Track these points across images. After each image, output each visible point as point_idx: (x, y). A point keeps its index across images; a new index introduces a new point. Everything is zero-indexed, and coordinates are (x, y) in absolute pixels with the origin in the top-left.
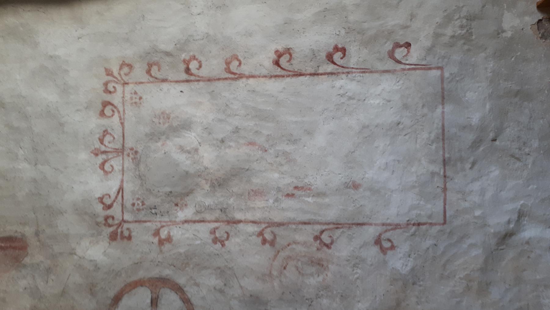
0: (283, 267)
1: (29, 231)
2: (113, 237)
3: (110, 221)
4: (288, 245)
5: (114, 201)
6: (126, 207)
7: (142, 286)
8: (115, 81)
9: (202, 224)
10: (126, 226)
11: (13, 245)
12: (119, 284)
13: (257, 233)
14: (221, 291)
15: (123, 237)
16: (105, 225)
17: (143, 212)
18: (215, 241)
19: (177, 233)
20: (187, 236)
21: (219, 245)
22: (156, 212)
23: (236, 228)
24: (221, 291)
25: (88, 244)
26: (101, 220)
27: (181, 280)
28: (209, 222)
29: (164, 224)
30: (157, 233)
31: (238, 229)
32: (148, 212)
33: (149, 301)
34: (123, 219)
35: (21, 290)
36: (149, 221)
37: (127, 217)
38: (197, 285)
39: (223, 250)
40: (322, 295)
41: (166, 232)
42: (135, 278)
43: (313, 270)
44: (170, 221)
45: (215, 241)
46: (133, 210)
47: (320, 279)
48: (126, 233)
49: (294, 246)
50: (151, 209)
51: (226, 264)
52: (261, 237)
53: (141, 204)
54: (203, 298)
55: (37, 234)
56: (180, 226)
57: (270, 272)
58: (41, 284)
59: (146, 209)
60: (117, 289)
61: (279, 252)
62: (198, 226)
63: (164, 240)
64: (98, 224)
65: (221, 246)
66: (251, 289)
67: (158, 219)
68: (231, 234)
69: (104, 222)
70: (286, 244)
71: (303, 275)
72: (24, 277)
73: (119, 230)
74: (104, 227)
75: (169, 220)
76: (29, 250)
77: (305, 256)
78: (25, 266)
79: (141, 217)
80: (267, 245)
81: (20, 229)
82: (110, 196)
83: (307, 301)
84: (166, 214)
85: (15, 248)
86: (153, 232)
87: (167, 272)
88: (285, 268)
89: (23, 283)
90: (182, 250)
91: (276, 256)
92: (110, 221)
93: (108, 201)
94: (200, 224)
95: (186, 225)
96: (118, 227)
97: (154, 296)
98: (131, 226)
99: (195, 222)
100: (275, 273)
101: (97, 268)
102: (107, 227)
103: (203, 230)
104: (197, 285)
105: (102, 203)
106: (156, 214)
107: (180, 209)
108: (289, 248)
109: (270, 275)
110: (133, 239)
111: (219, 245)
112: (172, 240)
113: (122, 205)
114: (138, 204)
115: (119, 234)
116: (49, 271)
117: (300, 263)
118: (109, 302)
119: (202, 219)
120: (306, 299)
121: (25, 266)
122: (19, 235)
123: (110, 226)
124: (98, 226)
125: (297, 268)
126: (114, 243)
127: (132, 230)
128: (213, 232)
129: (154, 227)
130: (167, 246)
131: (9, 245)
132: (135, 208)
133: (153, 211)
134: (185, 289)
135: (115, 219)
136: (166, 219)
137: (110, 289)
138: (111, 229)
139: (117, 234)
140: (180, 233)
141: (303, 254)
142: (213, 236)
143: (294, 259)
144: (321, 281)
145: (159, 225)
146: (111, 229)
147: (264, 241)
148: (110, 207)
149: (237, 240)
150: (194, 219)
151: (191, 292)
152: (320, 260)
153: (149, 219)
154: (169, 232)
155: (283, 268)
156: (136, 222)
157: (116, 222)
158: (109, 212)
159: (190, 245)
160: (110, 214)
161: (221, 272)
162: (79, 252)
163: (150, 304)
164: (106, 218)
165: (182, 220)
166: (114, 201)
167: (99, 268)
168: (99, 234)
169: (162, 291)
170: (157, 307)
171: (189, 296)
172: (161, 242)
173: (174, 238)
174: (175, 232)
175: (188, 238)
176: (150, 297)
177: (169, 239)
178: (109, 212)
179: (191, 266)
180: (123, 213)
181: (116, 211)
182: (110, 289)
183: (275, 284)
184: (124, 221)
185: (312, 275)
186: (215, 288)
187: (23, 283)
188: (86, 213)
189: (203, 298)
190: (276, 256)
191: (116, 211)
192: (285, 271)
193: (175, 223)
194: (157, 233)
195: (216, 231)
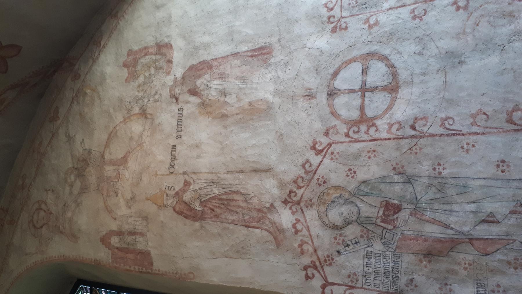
0: (476, 24)
1: (274, 40)
2: (334, 30)
3: (332, 19)
4: (481, 6)
5: (335, 5)
6: (343, 7)
7: (355, 62)
8: (85, 290)
9: (403, 8)
10: (343, 20)
11: (263, 52)
12: (337, 63)
13: (451, 3)
14: (420, 54)
15: (341, 29)
16: (328, 23)
17: (357, 9)
18: (414, 18)
19: (382, 18)
20: (391, 18)
21: (418, 20)
22: (367, 6)
23: (432, 5)
24: (420, 54)
25: (315, 38)
26: (325, 19)
27: (386, 51)
28: (409, 5)
29: (373, 13)
30: (367, 21)
31: (434, 4)
32: (361, 8)
33: (360, 71)
34: (341, 16)
35: (268, 81)
36: (361, 14)
37: (344, 14)
38: (399, 53)
39: (422, 23)
40: (514, 40)
41: (374, 19)
42: (349, 57)
43: (505, 21)
44: (377, 11)
45: (414, 18)
46: (349, 7)
47: (513, 26)
48: (344, 26)
49: (486, 6)
50: (362, 5)
51: (424, 33)
52: (455, 6)
53: (355, 3)
54: (404, 61)
55: (279, 41)
56: (385, 13)
57: (464, 31)
58: (280, 73)
59: (359, 5)
60: (336, 66)
61: (471, 13)
62: (400, 10)
63: (373, 25)
64: (323, 22)
65: (419, 21)
66: (446, 47)
67: (368, 11)
68: (429, 9)
69: (327, 21)
70: (478, 6)
71: (495, 27)
72: (270, 72)
73: (339, 25)
74: (327, 25)
75: (376, 10)
76: (274, 54)
77: (497, 12)
78: (270, 65)
79: (355, 11)
80: (461, 11)
81: (268, 40)
82: (332, 2)
83: (499, 47)
84: (374, 6)
85: (264, 54)
86: (364, 21)
87: (374, 48)
88: (477, 25)
89: (269, 76)
90: (387, 29)
91: (469, 17)
92: (332, 19)
93: (331, 6)
94: (401, 8)
95: (390, 11)
96: (338, 23)
97: (365, 67)
98: (347, 20)
99: (397, 8)
100: (468, 30)
101: (322, 53)
102: (330, 24)
103: (405, 12)
104: (399, 53)
105: (327, 7)
106: (366, 8)
107: (385, 1)
108: (481, 8)
109: (464, 33)
110: (349, 29)
111: (418, 20)
112: (379, 24)
113: (341, 6)
114: (353, 3)
115: (338, 27)
116: (286, 64)
117: (492, 18)
118: (330, 77)
119: (403, 5)
120: (499, 46)
121: (270, 65)
122: (267, 45)
123: (332, 23)
124: (324, 24)
125: (489, 22)
126: (335, 35)
127: (348, 22)
128: (413, 11)
129: (365, 17)
130: (375, 28)
131: (260, 53)
132: (350, 6)
133: (364, 6)
134: (389, 58)
135: (336, 17)
136: (374, 10)
137: (331, 68)
138: (333, 25)
139: (336, 28)
140: (386, 17)
141: (495, 10)
142: (412, 15)
143: (486, 16)
144: (513, 28)
145: (368, 15)
146: (333, 25)
147: (458, 8)
148: (332, 9)
149: (434, 13)
150: (396, 6)
151: (394, 59)
152: (511, 12)
153: (361, 13)
154: (376, 19)
155: (476, 25)
156: (351, 16)
157: (336, 19)
158: (332, 13)
159: (394, 24)
160: (332, 14)
161: (419, 40)
162: (309, 45)
163: (361, 74)
164: (329, 18)
165: (387, 8)
166: (335, 5)
167: (323, 54)
168: (324, 29)
169: (371, 62)
170: (367, 75)
171: (393, 61)
172: (370, 27)
173: (380, 22)
174: (381, 17)
175: (392, 20)
176: (361, 68)
177: (377, 23)
178: (332, 13)
179: (395, 40)
180: (341, 12)
181: (337, 12)
182: (331, 68)
183: (469, 39)
184: (342, 17)
185: (503, 25)
186: (414, 53)
187: (269, 76)
188: (314, 17)
189: (405, 62)
190: (469, 17)
191: (337, 12)
192: (478, 27)
193: (381, 12)
194: (367, 21)
195: (415, 10)
